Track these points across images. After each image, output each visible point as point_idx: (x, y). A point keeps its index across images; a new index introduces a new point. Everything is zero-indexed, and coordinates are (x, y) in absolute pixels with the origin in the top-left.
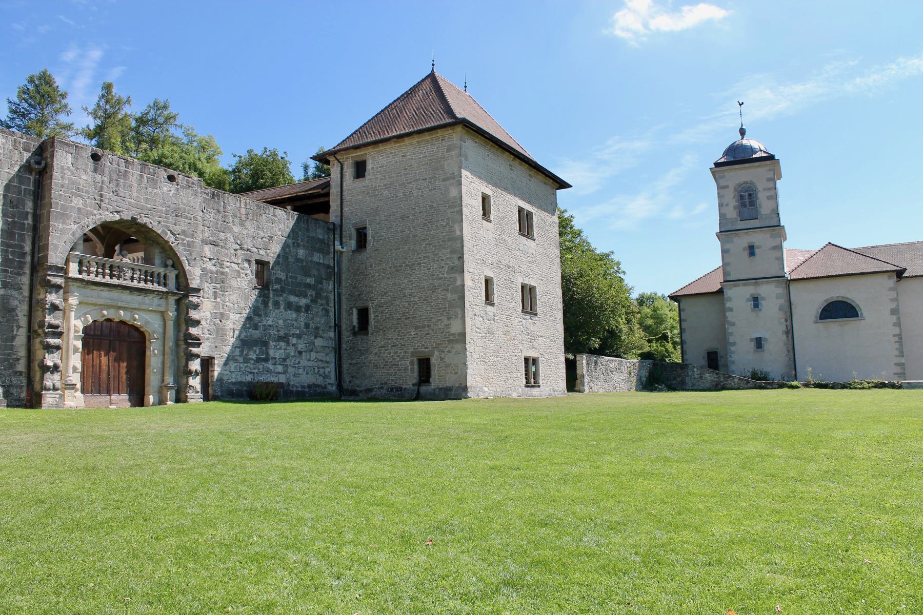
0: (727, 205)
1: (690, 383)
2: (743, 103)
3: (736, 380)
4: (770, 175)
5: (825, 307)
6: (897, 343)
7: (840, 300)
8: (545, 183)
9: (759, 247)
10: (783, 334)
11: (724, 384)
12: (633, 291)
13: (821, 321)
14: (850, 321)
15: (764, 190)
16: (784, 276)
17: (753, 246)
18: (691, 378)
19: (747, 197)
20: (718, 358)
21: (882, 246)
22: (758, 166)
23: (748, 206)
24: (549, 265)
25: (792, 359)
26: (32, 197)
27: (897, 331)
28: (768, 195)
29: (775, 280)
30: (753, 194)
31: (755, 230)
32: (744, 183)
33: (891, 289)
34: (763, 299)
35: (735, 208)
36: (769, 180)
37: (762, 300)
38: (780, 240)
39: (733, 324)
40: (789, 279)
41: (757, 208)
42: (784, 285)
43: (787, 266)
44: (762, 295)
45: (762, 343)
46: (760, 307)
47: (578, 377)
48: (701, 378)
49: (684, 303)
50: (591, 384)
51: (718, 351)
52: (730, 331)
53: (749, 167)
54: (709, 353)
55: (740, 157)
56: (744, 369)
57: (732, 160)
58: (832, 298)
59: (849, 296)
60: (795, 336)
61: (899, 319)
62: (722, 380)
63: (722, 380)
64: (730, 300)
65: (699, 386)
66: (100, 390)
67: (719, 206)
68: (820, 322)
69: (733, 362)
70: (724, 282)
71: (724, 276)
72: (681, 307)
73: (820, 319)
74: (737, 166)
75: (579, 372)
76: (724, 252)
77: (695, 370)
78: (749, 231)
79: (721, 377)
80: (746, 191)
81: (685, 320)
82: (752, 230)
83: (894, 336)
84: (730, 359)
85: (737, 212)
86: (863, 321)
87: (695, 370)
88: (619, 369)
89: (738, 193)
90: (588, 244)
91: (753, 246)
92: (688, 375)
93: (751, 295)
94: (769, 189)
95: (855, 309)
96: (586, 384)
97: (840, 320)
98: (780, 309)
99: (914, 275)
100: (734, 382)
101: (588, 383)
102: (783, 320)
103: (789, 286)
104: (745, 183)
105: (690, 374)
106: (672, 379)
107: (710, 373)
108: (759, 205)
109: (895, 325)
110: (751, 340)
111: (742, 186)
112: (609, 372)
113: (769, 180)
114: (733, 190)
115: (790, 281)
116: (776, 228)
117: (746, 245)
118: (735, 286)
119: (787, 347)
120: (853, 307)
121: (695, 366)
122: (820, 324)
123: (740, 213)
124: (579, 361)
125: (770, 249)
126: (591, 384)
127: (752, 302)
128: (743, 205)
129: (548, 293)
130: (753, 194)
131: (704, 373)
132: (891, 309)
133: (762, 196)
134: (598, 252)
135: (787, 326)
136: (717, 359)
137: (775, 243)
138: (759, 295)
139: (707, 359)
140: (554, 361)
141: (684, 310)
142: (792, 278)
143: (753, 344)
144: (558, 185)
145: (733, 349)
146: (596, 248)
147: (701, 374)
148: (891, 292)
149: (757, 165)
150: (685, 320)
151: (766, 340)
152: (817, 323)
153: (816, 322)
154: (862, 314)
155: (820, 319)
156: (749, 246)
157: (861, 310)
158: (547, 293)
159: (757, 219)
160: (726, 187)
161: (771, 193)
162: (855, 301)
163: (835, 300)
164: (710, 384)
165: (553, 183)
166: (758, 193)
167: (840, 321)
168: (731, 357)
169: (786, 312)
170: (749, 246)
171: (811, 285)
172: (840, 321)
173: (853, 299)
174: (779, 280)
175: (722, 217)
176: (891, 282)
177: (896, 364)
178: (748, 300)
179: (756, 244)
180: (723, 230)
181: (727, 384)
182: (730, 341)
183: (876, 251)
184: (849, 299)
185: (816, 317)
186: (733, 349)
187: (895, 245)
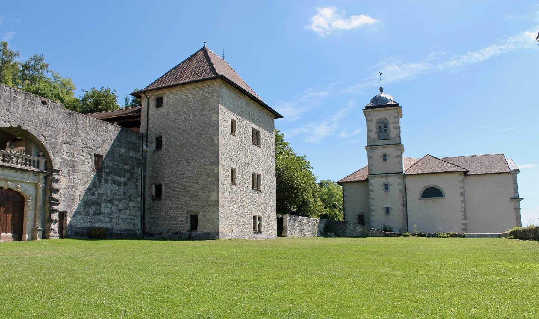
0: (372, 131)
2: (382, 73)
3: (374, 231)
4: (396, 115)
9: (389, 156)
10: (401, 205)
12: (317, 179)
15: (393, 123)
16: (403, 173)
19: (383, 127)
21: (456, 157)
25: (406, 220)
27: (463, 205)
28: (394, 126)
30: (386, 125)
33: (460, 182)
34: (391, 185)
35: (376, 133)
36: (396, 117)
39: (373, 199)
42: (402, 178)
44: (390, 183)
47: (284, 228)
48: (354, 229)
49: (346, 186)
50: (292, 232)
51: (365, 214)
52: (371, 203)
54: (359, 215)
57: (375, 105)
58: (429, 185)
59: (438, 185)
62: (366, 231)
63: (366, 231)
64: (372, 186)
67: (367, 131)
69: (373, 221)
74: (378, 109)
76: (369, 158)
77: (351, 225)
78: (384, 146)
79: (366, 230)
80: (382, 123)
81: (346, 196)
82: (385, 146)
83: (462, 208)
84: (371, 219)
85: (377, 135)
89: (378, 124)
92: (347, 228)
93: (384, 183)
94: (395, 123)
95: (441, 192)
98: (400, 191)
100: (373, 233)
102: (401, 198)
103: (405, 178)
104: (382, 119)
105: (348, 227)
107: (360, 227)
108: (390, 132)
109: (462, 201)
110: (383, 208)
111: (381, 120)
113: (396, 117)
117: (382, 154)
118: (375, 177)
119: (403, 213)
122: (422, 200)
123: (379, 136)
125: (395, 157)
126: (292, 232)
128: (381, 131)
130: (386, 125)
132: (461, 193)
133: (391, 127)
134: (297, 155)
135: (403, 201)
137: (398, 153)
138: (389, 183)
143: (384, 211)
144: (276, 116)
145: (372, 213)
149: (389, 109)
150: (346, 196)
151: (392, 209)
153: (419, 199)
154: (445, 195)
157: (444, 193)
159: (388, 139)
160: (371, 121)
161: (397, 125)
162: (442, 188)
168: (371, 218)
171: (417, 178)
173: (440, 186)
176: (461, 177)
178: (382, 186)
179: (387, 154)
180: (369, 145)
183: (453, 160)
184: (438, 186)
185: (420, 196)
186: (372, 213)
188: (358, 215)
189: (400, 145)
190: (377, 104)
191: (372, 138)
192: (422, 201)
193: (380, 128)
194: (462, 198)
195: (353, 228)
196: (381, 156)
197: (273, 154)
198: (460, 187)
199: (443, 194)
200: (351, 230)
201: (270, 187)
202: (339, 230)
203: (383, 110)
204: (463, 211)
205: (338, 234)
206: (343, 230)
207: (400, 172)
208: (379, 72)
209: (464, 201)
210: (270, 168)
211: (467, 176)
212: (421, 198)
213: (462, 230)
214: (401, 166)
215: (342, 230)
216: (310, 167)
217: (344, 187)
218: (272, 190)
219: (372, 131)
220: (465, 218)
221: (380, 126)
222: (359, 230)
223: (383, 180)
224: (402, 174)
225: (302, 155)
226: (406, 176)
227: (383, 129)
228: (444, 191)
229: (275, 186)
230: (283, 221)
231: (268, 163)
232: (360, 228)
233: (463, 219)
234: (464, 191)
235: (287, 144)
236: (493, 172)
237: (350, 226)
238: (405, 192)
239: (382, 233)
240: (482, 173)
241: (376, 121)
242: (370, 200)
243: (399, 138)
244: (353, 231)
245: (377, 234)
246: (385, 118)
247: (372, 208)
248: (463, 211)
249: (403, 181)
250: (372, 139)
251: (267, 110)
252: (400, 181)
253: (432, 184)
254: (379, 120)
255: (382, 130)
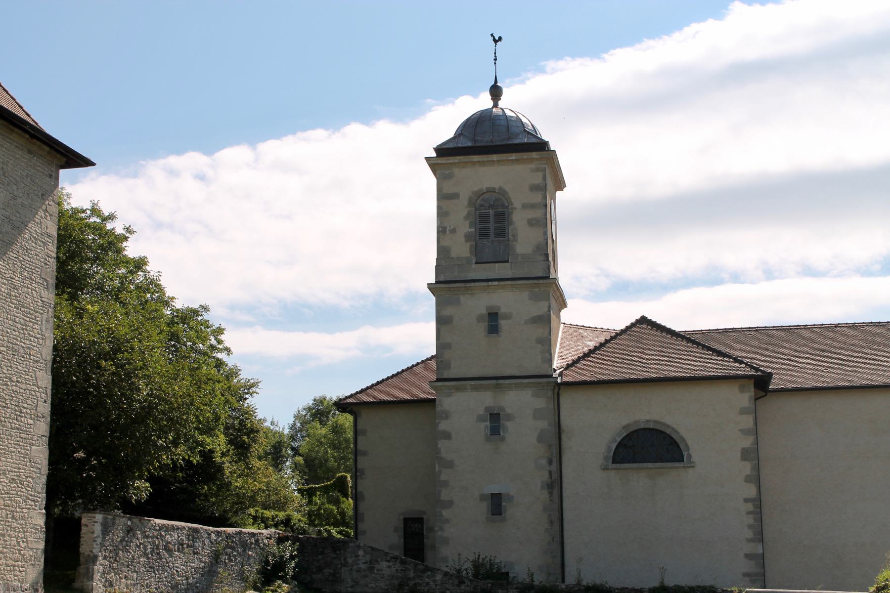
0: (453, 231)
1: (349, 580)
2: (500, 39)
3: (439, 577)
4: (537, 179)
5: (623, 439)
6: (752, 516)
7: (651, 427)
8: (30, 152)
9: (508, 317)
10: (542, 488)
11: (415, 584)
12: (257, 390)
13: (615, 465)
14: (668, 468)
15: (525, 206)
16: (551, 376)
17: (497, 314)
18: (351, 570)
19: (492, 219)
20: (425, 533)
21: (742, 330)
22: (516, 160)
23: (492, 235)
24: (23, 322)
25: (558, 539)
26: (55, 192)
27: (752, 491)
28: (530, 217)
29: (534, 383)
30: (503, 214)
31: (502, 283)
32: (487, 192)
33: (743, 411)
34: (509, 417)
35: (468, 237)
36: (534, 188)
37: (509, 420)
38: (547, 304)
39: (450, 465)
40: (559, 381)
41: (508, 240)
42: (550, 393)
43: (561, 357)
44: (509, 410)
45: (503, 504)
46: (502, 434)
47: (82, 559)
48: (371, 569)
49: (366, 416)
50: (111, 576)
51: (425, 517)
52: (443, 477)
53: (498, 161)
54: (406, 520)
55: (485, 140)
56: (459, 555)
57: (469, 144)
58: (636, 422)
59: (668, 420)
60: (564, 494)
61: (757, 468)
62: (412, 574)
63: (412, 574)
64: (447, 417)
65: (367, 586)
66: (765, 586)
67: (438, 232)
68: (612, 469)
69: (446, 541)
70: (438, 380)
71: (438, 369)
72: (359, 427)
73: (613, 463)
74: (476, 158)
75: (84, 549)
76: (442, 321)
77: (361, 553)
78: (490, 283)
79: (410, 570)
80: (491, 207)
81: (365, 454)
82: (496, 283)
83: (746, 500)
84: (440, 533)
85: (471, 246)
86: (690, 471)
87: (361, 553)
88: (188, 546)
89: (476, 209)
90: (159, 288)
91: (497, 314)
92: (345, 564)
93: (487, 409)
94: (533, 206)
95: (679, 447)
96: (97, 576)
97: (650, 465)
98: (540, 439)
99: (789, 386)
100: (435, 581)
101: (104, 573)
102: (544, 462)
103: (558, 395)
104: (490, 190)
105: (350, 561)
106: (314, 570)
107: (389, 561)
108: (513, 236)
109: (748, 479)
110: (483, 497)
111: (486, 196)
112: (164, 553)
113: (534, 188)
114: (466, 203)
115: (559, 384)
116: (541, 281)
117: (484, 311)
118: (458, 389)
119: (550, 515)
120: (676, 442)
121: (362, 545)
122: (612, 473)
123: (476, 250)
124: (86, 526)
125: (526, 322)
126: (111, 576)
127: (488, 423)
128: (483, 234)
129: (15, 379)
130: (503, 214)
131: (377, 561)
132: (743, 449)
133: (519, 219)
134: (178, 305)
135: (550, 472)
136: (423, 534)
137: (538, 309)
138: (503, 409)
139: (402, 533)
140: (14, 525)
141: (364, 433)
142: (565, 379)
143: (484, 507)
144: (65, 160)
145: (445, 513)
146: (173, 298)
147: (371, 562)
148: (744, 416)
149: (513, 158)
150: (365, 454)
151: (510, 498)
152: (608, 469)
153: (605, 469)
154: (690, 456)
155: (613, 463)
156: (489, 314)
157: (688, 448)
158: (10, 378)
159: (507, 262)
160: (454, 196)
161: (537, 214)
162: (679, 430)
163: (642, 427)
164: (387, 582)
165: (49, 153)
166: (512, 213)
167: (650, 469)
168: (441, 529)
169: (550, 446)
170: (489, 314)
171: (599, 396)
172: (650, 469)
173: (675, 426)
174: (540, 383)
175: (443, 252)
176: (744, 398)
177: (747, 556)
178: (480, 419)
179: (503, 310)
180: (442, 279)
181: (420, 585)
182: (442, 498)
183: (730, 338)
184: (668, 426)
185: (606, 458)
186: (445, 513)
187: (766, 329)
188: (402, 517)
189: (545, 281)
190: (475, 141)
191: (453, 254)
192: (612, 473)
193: (480, 222)
194: (747, 468)
195: (366, 563)
196: (480, 319)
197: (45, 294)
198: (741, 430)
199: (685, 454)
200: (359, 571)
201: (24, 410)
202: (320, 570)
203: (493, 161)
204: (748, 513)
205: (315, 586)
206: (332, 571)
207: (543, 373)
208: (492, 35)
209: (756, 478)
210: (28, 342)
211: (769, 394)
212: (611, 466)
213: (747, 579)
214: (548, 355)
215: (326, 571)
216: (221, 347)
217: (359, 420)
218: (31, 422)
219: (453, 231)
220: (759, 536)
221: (481, 216)
222: (387, 572)
223: (484, 399)
224: (550, 380)
225: (195, 306)
226: (562, 387)
227: (492, 225)
228: (689, 444)
229: (45, 409)
230: (79, 535)
231: (19, 326)
232: (391, 564)
233: (749, 540)
234: (611, 443)
235: (140, 264)
236: (858, 384)
237: (357, 556)
238: (558, 441)
239: (463, 582)
240: (820, 385)
241: (470, 200)
242: (437, 469)
243: (542, 258)
244: (366, 576)
245: (447, 586)
246: (500, 188)
247: (445, 495)
248: (748, 513)
249: (551, 406)
250: (453, 258)
251: (27, 136)
252: (541, 403)
253: (648, 418)
254: (480, 194)
255: (489, 228)
